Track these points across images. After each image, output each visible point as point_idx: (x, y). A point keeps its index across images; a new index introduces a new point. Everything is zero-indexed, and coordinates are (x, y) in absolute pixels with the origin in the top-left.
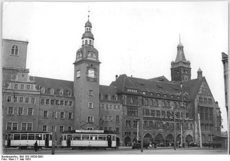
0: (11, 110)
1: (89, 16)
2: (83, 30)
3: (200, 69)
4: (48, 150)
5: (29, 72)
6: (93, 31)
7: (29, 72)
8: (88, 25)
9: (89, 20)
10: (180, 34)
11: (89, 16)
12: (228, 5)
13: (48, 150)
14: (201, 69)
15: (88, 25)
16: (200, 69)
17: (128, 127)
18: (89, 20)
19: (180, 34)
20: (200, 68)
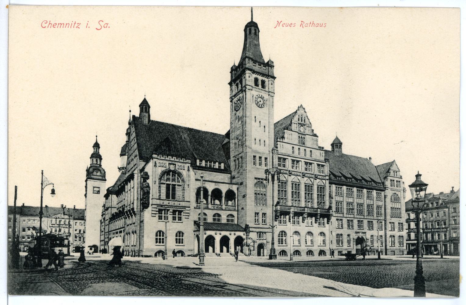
0: (159, 236)
1: (97, 136)
2: (91, 151)
3: (337, 138)
4: (246, 97)
5: (104, 197)
6: (101, 152)
7: (104, 197)
8: (97, 145)
9: (97, 141)
10: (325, 287)
11: (97, 136)
12: (212, 272)
13: (246, 97)
14: (340, 138)
15: (97, 145)
16: (337, 138)
17: (437, 232)
18: (97, 141)
19: (325, 287)
20: (145, 99)
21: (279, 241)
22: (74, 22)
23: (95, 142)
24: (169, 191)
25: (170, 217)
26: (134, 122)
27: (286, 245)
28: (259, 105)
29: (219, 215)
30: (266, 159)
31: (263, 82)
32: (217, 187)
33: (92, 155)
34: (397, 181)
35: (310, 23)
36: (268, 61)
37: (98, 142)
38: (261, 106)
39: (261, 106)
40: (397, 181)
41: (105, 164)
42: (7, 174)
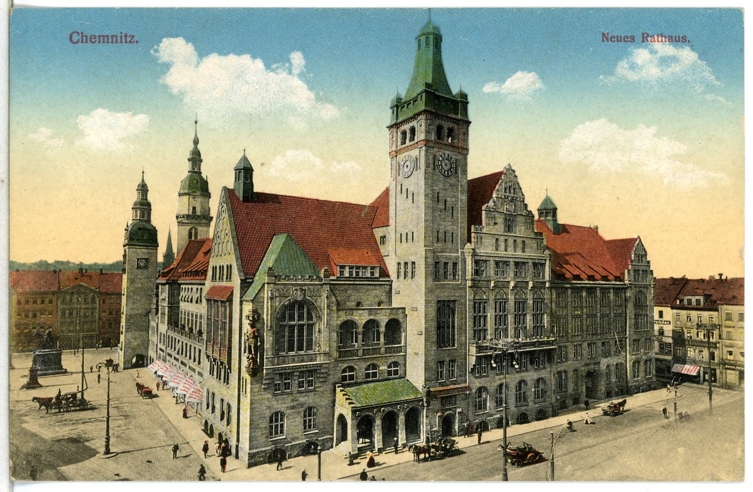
6: (150, 198)
8: (143, 189)
9: (143, 180)
10: (401, 242)
11: (143, 172)
15: (143, 189)
19: (401, 242)
21: (476, 406)
23: (140, 181)
24: (298, 340)
26: (210, 197)
27: (524, 403)
28: (445, 173)
29: (351, 369)
30: (455, 264)
31: (451, 132)
33: (135, 204)
34: (643, 271)
36: (491, 180)
38: (448, 174)
39: (448, 174)
40: (643, 271)
41: (156, 220)
42: (7, 166)
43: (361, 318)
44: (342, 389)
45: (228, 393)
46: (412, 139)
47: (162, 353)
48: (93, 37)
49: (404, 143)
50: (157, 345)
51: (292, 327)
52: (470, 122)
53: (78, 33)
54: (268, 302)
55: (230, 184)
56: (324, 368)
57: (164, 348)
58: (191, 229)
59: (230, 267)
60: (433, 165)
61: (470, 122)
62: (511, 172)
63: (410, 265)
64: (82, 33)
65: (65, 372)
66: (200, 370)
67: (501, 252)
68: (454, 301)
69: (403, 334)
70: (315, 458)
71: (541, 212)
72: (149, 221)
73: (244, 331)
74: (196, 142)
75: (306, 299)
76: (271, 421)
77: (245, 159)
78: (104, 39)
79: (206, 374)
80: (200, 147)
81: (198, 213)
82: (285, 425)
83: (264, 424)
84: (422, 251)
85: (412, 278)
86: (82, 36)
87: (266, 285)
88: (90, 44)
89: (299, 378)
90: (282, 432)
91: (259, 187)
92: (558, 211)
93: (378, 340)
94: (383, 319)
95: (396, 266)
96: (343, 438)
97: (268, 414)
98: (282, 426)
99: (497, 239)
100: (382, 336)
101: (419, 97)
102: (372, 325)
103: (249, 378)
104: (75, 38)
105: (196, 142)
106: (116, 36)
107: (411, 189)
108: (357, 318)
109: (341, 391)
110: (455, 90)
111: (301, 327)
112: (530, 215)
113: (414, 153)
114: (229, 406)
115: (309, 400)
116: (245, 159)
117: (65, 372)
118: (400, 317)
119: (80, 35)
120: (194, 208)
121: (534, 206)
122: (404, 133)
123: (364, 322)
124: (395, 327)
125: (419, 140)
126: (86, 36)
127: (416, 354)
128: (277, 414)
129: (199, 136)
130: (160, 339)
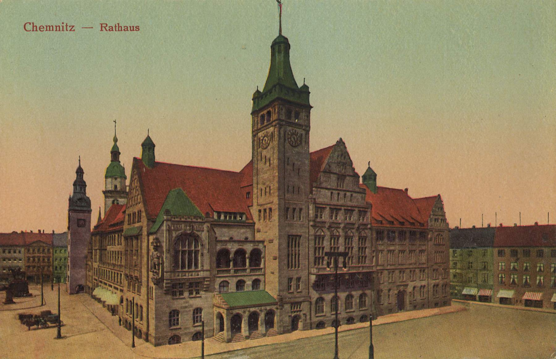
6: (85, 178)
8: (80, 172)
15: (80, 172)
22: (65, 25)
25: (186, 294)
32: (241, 247)
35: (116, 27)
37: (82, 166)
40: (441, 220)
41: (89, 192)
43: (233, 248)
44: (219, 295)
45: (140, 300)
46: (268, 120)
47: (95, 281)
48: (42, 27)
49: (262, 123)
50: (92, 276)
51: (184, 252)
52: (312, 107)
53: (30, 24)
54: (166, 234)
55: (139, 154)
56: (207, 281)
57: (97, 278)
58: (113, 201)
59: (140, 212)
60: (284, 139)
61: (312, 107)
62: (341, 143)
63: (268, 211)
64: (33, 23)
65: (31, 295)
66: (121, 288)
67: (335, 202)
68: (300, 236)
69: (263, 260)
70: (200, 342)
71: (364, 177)
72: (85, 193)
73: (151, 254)
74: (116, 140)
75: (194, 233)
76: (170, 317)
77: (148, 138)
78: (50, 29)
79: (125, 289)
80: (118, 144)
81: (119, 189)
82: (180, 319)
83: (166, 318)
84: (276, 200)
85: (270, 219)
86: (33, 27)
87: (165, 222)
88: (39, 32)
89: (190, 288)
90: (178, 324)
91: (159, 158)
92: (377, 178)
93: (244, 264)
94: (249, 248)
95: (258, 213)
96: (222, 329)
97: (168, 311)
98: (178, 320)
99: (332, 193)
100: (247, 261)
101: (274, 89)
102: (241, 253)
103: (154, 286)
104: (29, 27)
105: (116, 140)
106: (59, 26)
107: (268, 157)
108: (230, 247)
109: (219, 297)
110: (300, 84)
111: (190, 253)
112: (356, 176)
113: (271, 129)
114: (141, 307)
115: (196, 303)
116: (148, 138)
117: (31, 295)
118: (261, 246)
119: (32, 24)
120: (116, 187)
121: (361, 170)
122: (263, 116)
123: (235, 249)
124: (256, 256)
125: (274, 119)
126: (36, 26)
127: (273, 273)
128: (174, 311)
129: (117, 137)
130: (94, 273)
